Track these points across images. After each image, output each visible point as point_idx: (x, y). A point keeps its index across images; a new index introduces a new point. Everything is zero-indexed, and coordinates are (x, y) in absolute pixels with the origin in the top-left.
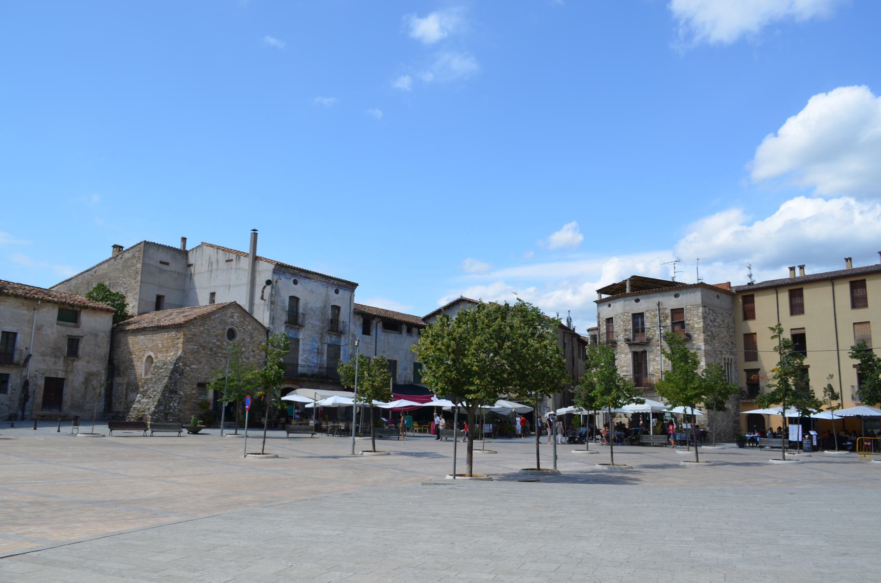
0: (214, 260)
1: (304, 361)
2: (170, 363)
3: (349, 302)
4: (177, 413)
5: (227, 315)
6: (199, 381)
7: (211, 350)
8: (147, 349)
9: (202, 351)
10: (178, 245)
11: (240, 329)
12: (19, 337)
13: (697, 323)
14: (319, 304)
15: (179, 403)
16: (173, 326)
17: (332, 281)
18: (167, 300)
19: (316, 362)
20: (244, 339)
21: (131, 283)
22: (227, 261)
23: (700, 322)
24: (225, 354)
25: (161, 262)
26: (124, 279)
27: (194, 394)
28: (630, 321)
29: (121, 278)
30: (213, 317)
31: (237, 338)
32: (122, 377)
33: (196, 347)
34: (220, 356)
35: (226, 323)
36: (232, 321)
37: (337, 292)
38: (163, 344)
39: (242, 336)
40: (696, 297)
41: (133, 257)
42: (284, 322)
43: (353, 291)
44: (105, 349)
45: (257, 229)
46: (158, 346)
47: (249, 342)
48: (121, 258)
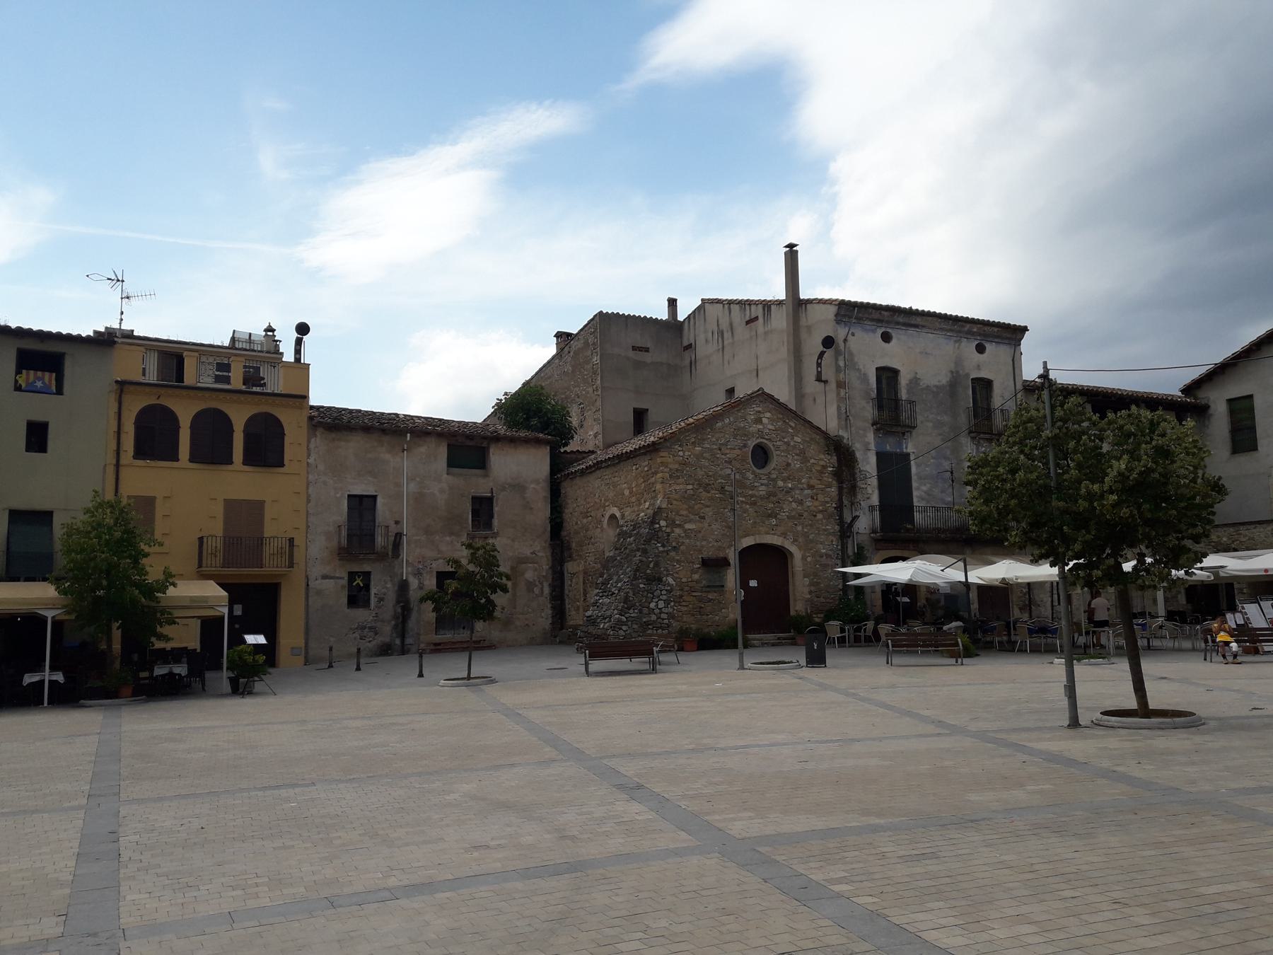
0: (724, 325)
1: (923, 499)
2: (644, 522)
3: (1011, 369)
4: (666, 621)
5: (748, 417)
6: (705, 555)
7: (722, 489)
8: (607, 504)
9: (704, 494)
10: (663, 314)
11: (778, 443)
12: (380, 501)
14: (944, 379)
15: (667, 602)
17: (968, 326)
18: (651, 417)
19: (950, 499)
20: (788, 465)
22: (748, 323)
24: (752, 496)
25: (634, 348)
27: (697, 582)
30: (719, 424)
31: (772, 465)
32: (576, 560)
33: (691, 487)
34: (742, 502)
37: (980, 349)
38: (630, 489)
41: (586, 344)
42: (871, 422)
43: (1017, 343)
44: (542, 512)
45: (796, 243)
47: (800, 470)
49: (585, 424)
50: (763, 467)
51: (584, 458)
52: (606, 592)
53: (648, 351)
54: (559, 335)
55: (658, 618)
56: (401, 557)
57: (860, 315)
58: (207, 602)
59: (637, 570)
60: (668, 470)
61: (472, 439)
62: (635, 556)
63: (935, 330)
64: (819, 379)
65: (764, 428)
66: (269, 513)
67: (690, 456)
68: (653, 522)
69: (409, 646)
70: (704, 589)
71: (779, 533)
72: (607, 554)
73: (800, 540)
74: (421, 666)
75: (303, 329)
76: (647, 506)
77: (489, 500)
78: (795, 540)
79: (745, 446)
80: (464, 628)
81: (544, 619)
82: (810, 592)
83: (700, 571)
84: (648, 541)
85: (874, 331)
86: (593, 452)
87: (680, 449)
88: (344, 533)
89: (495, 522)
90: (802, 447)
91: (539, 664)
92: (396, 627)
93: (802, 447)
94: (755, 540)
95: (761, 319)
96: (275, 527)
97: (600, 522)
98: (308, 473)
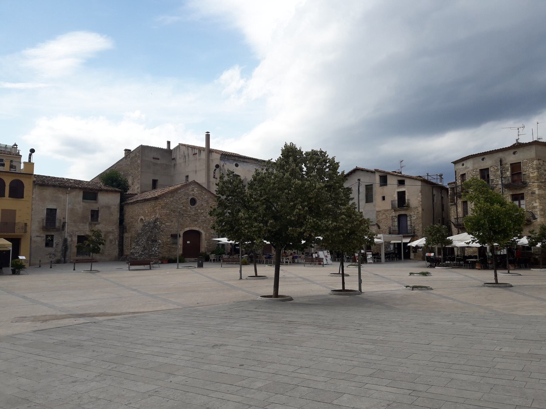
6: (172, 233)
9: (173, 214)
10: (165, 147)
12: (58, 211)
13: (532, 173)
15: (158, 248)
16: (152, 199)
18: (159, 183)
20: (202, 205)
21: (135, 173)
22: (194, 155)
23: (535, 172)
24: (189, 214)
25: (154, 158)
26: (132, 171)
27: (169, 242)
28: (478, 175)
29: (130, 170)
30: (179, 191)
31: (197, 205)
32: (128, 233)
33: (168, 211)
34: (186, 216)
35: (189, 195)
36: (193, 194)
38: (148, 211)
39: (201, 203)
40: (531, 153)
41: (136, 155)
46: (146, 212)
47: (206, 206)
48: (129, 157)
49: (134, 184)
50: (194, 205)
51: (133, 196)
52: (137, 244)
53: (159, 159)
54: (126, 150)
55: (155, 253)
56: (65, 230)
57: (228, 158)
58: (5, 246)
59: (148, 238)
60: (161, 206)
61: (92, 190)
62: (148, 233)
63: (253, 163)
64: (214, 177)
65: (195, 193)
66: (18, 214)
67: (169, 201)
68: (155, 222)
69: (67, 261)
70: (171, 244)
71: (198, 226)
72: (139, 232)
73: (205, 229)
74: (74, 267)
75: (32, 151)
76: (153, 217)
77: (97, 211)
78: (203, 229)
79: (188, 199)
80: (86, 255)
81: (116, 253)
82: (207, 245)
83: (170, 238)
84: (153, 228)
85: (233, 163)
86: (136, 194)
87: (165, 199)
88: (45, 221)
89: (99, 219)
90: (207, 199)
91: (114, 267)
92: (62, 254)
93: (207, 199)
94: (190, 228)
95: (198, 154)
96: (20, 219)
97: (137, 220)
98: (32, 201)
